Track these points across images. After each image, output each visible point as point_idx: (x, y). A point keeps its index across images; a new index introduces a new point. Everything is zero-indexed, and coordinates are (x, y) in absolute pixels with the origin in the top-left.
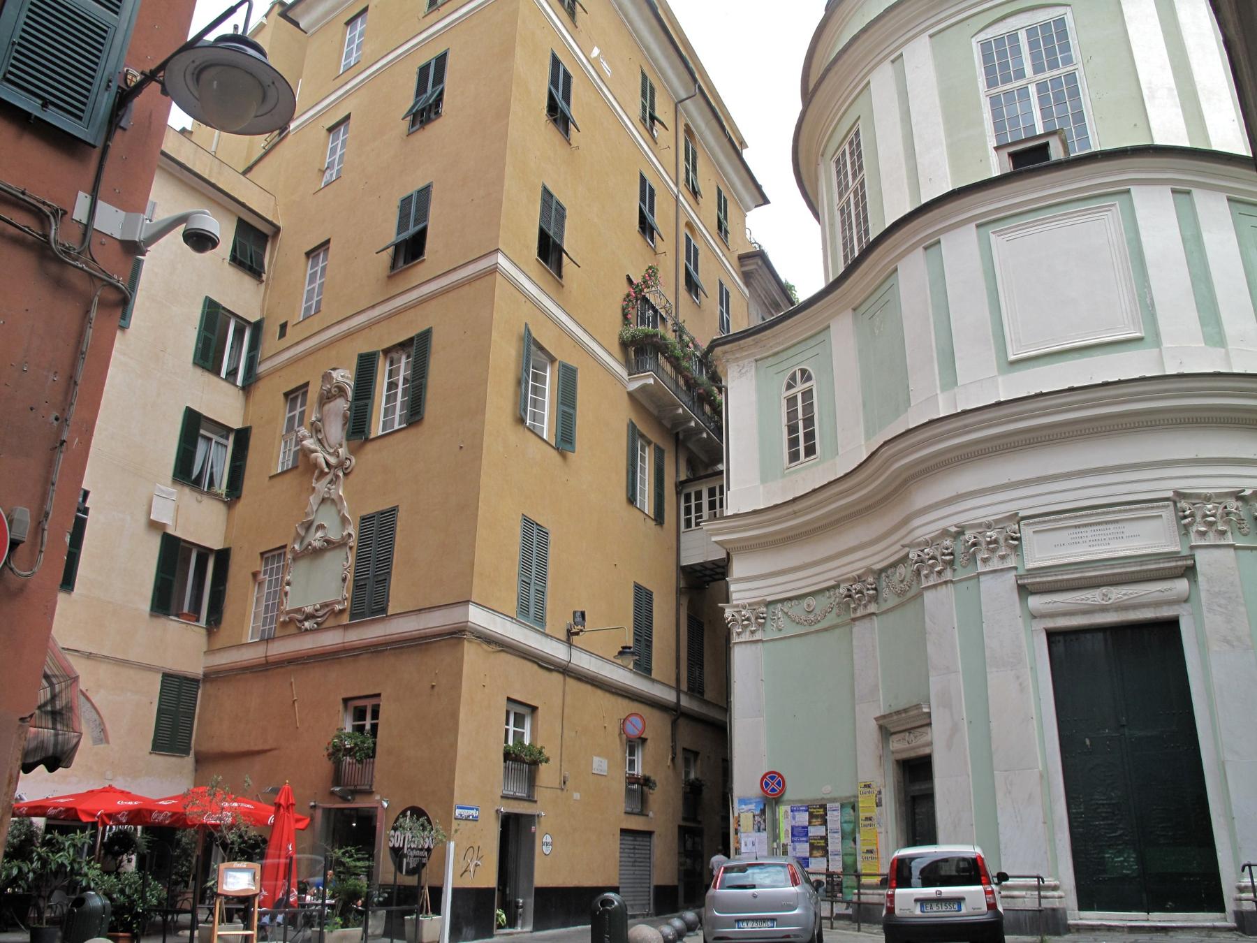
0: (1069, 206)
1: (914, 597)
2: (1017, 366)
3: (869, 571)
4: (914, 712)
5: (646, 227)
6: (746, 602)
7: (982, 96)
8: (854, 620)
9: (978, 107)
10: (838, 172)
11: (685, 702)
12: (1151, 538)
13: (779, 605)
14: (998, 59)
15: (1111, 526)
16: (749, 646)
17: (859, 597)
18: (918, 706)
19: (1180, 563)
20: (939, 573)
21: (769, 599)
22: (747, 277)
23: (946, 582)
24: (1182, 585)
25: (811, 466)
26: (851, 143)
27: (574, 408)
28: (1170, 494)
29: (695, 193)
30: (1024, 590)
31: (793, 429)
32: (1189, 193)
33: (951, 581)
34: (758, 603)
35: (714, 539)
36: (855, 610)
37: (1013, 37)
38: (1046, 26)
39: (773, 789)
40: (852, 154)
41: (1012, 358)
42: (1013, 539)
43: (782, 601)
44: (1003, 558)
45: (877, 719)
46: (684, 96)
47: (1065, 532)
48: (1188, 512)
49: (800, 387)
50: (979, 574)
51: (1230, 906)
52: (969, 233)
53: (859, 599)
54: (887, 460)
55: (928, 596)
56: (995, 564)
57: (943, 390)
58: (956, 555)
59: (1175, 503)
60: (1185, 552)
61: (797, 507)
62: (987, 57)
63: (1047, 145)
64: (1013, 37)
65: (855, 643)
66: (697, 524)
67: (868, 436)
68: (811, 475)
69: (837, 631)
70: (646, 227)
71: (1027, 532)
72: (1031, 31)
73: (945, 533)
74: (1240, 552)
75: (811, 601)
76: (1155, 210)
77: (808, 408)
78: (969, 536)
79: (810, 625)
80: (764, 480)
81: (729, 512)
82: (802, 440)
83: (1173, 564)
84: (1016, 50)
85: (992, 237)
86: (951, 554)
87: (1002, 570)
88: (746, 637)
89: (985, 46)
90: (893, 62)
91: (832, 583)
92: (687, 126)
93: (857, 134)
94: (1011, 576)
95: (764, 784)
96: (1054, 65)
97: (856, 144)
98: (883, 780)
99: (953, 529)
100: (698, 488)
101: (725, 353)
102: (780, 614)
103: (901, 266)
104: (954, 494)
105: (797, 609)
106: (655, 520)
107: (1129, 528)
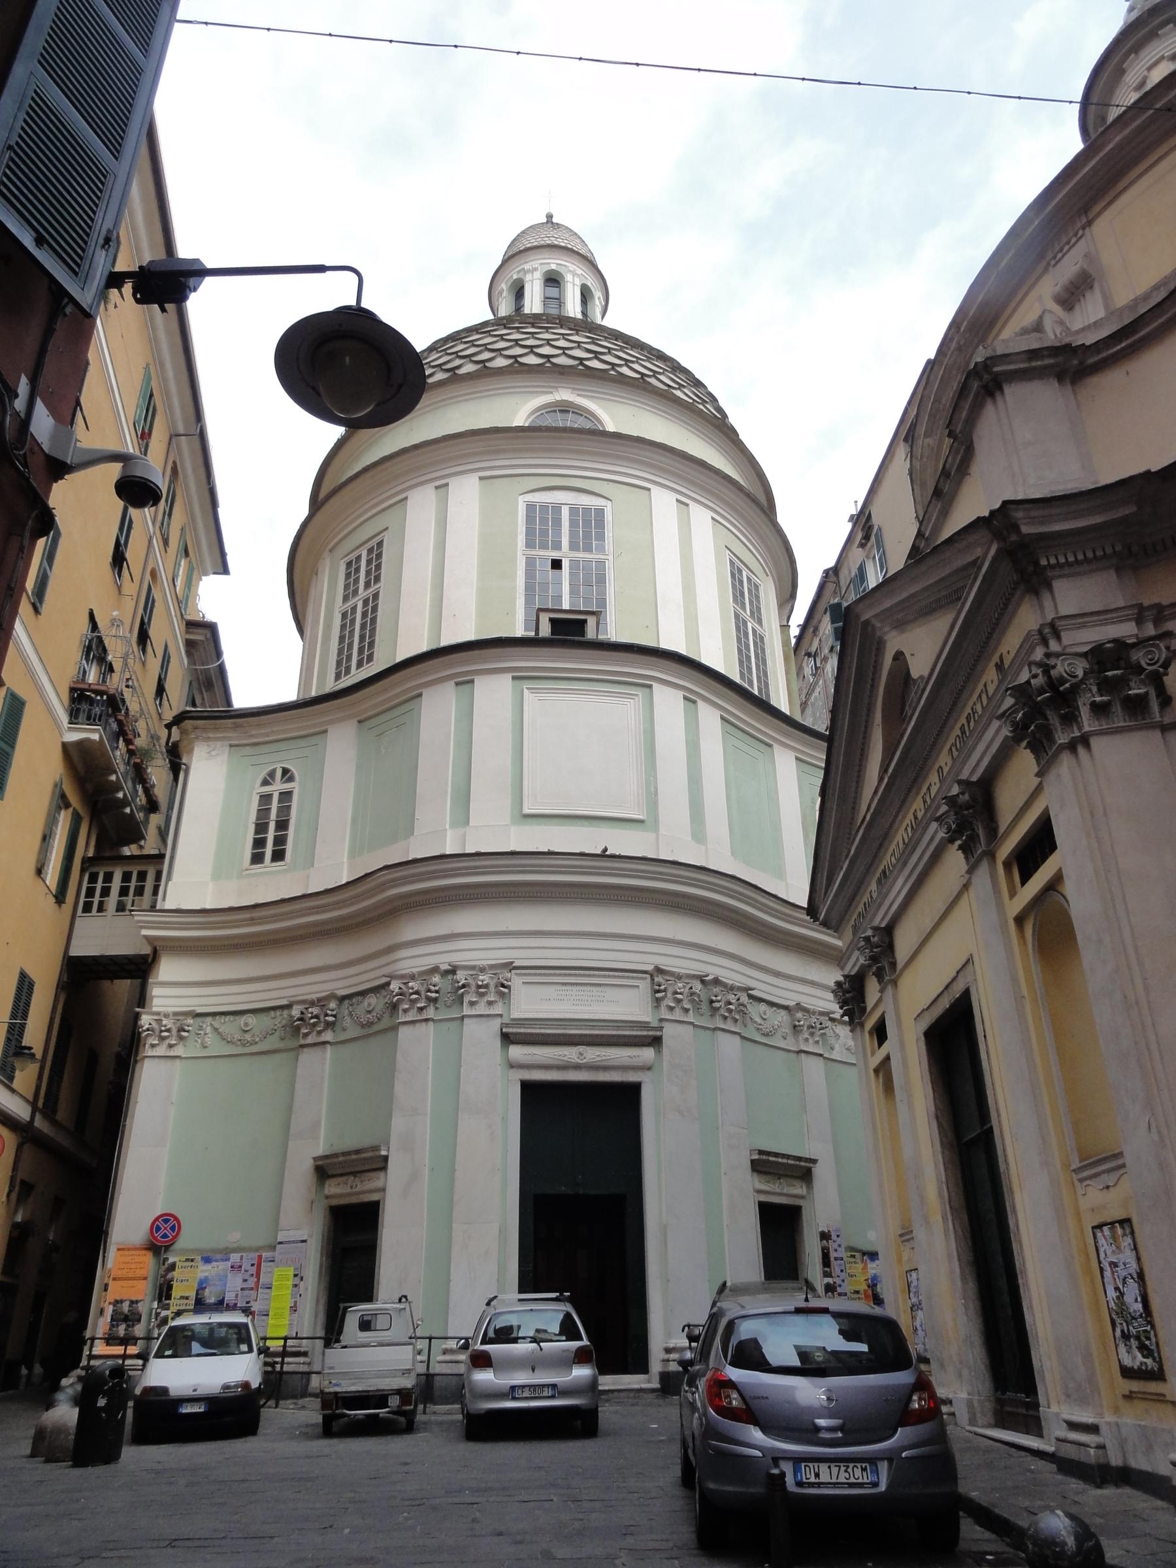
0: (628, 687)
1: (385, 1031)
2: (530, 820)
3: (332, 996)
4: (370, 1154)
5: (119, 559)
6: (170, 1010)
7: (519, 553)
8: (302, 1046)
9: (514, 560)
10: (348, 575)
11: (39, 1122)
12: (627, 1005)
13: (209, 1019)
14: (541, 524)
15: (574, 988)
16: (162, 1061)
17: (303, 1027)
18: (376, 1148)
19: (651, 1033)
20: (421, 1009)
21: (199, 1010)
22: (190, 645)
23: (427, 1020)
24: (648, 1054)
25: (277, 872)
26: (370, 551)
27: (13, 747)
28: (650, 968)
29: (166, 542)
30: (507, 1039)
31: (261, 828)
32: (650, 687)
33: (432, 1020)
34: (186, 1014)
35: (145, 932)
36: (306, 1035)
37: (557, 509)
38: (587, 510)
39: (162, 1238)
40: (369, 562)
41: (526, 811)
42: (503, 986)
43: (214, 1014)
44: (490, 1003)
45: (315, 1159)
46: (182, 431)
47: (552, 988)
48: (662, 987)
49: (278, 787)
50: (463, 1018)
51: (656, 1367)
52: (504, 683)
53: (314, 1025)
54: (384, 884)
55: (403, 1032)
56: (481, 1009)
57: (454, 824)
58: (449, 992)
59: (652, 976)
60: (655, 1024)
61: (257, 914)
62: (530, 519)
63: (585, 621)
64: (557, 509)
65: (299, 1071)
66: (121, 908)
67: (354, 852)
68: (274, 884)
69: (278, 1056)
70: (119, 559)
71: (516, 982)
72: (574, 511)
73: (435, 970)
74: (700, 1031)
75: (251, 1020)
76: (668, 702)
77: (285, 810)
78: (461, 976)
79: (244, 1045)
80: (217, 875)
81: (169, 904)
82: (270, 840)
83: (645, 1033)
84: (557, 522)
85: (526, 691)
86: (437, 992)
87: (488, 1016)
88: (161, 1051)
89: (530, 507)
90: (437, 488)
91: (284, 1002)
92: (174, 463)
93: (380, 544)
94: (497, 1023)
95: (155, 1227)
96: (588, 548)
97: (376, 553)
98: (303, 1228)
99: (444, 967)
100: (109, 869)
101: (196, 728)
102: (209, 1030)
103: (427, 694)
104: (449, 932)
105: (229, 1027)
106: (56, 897)
107: (611, 993)
